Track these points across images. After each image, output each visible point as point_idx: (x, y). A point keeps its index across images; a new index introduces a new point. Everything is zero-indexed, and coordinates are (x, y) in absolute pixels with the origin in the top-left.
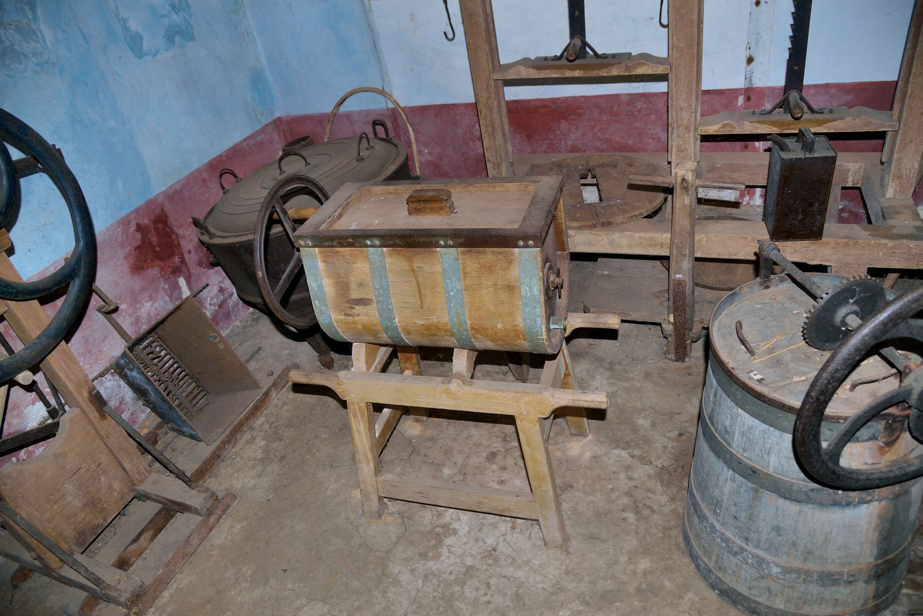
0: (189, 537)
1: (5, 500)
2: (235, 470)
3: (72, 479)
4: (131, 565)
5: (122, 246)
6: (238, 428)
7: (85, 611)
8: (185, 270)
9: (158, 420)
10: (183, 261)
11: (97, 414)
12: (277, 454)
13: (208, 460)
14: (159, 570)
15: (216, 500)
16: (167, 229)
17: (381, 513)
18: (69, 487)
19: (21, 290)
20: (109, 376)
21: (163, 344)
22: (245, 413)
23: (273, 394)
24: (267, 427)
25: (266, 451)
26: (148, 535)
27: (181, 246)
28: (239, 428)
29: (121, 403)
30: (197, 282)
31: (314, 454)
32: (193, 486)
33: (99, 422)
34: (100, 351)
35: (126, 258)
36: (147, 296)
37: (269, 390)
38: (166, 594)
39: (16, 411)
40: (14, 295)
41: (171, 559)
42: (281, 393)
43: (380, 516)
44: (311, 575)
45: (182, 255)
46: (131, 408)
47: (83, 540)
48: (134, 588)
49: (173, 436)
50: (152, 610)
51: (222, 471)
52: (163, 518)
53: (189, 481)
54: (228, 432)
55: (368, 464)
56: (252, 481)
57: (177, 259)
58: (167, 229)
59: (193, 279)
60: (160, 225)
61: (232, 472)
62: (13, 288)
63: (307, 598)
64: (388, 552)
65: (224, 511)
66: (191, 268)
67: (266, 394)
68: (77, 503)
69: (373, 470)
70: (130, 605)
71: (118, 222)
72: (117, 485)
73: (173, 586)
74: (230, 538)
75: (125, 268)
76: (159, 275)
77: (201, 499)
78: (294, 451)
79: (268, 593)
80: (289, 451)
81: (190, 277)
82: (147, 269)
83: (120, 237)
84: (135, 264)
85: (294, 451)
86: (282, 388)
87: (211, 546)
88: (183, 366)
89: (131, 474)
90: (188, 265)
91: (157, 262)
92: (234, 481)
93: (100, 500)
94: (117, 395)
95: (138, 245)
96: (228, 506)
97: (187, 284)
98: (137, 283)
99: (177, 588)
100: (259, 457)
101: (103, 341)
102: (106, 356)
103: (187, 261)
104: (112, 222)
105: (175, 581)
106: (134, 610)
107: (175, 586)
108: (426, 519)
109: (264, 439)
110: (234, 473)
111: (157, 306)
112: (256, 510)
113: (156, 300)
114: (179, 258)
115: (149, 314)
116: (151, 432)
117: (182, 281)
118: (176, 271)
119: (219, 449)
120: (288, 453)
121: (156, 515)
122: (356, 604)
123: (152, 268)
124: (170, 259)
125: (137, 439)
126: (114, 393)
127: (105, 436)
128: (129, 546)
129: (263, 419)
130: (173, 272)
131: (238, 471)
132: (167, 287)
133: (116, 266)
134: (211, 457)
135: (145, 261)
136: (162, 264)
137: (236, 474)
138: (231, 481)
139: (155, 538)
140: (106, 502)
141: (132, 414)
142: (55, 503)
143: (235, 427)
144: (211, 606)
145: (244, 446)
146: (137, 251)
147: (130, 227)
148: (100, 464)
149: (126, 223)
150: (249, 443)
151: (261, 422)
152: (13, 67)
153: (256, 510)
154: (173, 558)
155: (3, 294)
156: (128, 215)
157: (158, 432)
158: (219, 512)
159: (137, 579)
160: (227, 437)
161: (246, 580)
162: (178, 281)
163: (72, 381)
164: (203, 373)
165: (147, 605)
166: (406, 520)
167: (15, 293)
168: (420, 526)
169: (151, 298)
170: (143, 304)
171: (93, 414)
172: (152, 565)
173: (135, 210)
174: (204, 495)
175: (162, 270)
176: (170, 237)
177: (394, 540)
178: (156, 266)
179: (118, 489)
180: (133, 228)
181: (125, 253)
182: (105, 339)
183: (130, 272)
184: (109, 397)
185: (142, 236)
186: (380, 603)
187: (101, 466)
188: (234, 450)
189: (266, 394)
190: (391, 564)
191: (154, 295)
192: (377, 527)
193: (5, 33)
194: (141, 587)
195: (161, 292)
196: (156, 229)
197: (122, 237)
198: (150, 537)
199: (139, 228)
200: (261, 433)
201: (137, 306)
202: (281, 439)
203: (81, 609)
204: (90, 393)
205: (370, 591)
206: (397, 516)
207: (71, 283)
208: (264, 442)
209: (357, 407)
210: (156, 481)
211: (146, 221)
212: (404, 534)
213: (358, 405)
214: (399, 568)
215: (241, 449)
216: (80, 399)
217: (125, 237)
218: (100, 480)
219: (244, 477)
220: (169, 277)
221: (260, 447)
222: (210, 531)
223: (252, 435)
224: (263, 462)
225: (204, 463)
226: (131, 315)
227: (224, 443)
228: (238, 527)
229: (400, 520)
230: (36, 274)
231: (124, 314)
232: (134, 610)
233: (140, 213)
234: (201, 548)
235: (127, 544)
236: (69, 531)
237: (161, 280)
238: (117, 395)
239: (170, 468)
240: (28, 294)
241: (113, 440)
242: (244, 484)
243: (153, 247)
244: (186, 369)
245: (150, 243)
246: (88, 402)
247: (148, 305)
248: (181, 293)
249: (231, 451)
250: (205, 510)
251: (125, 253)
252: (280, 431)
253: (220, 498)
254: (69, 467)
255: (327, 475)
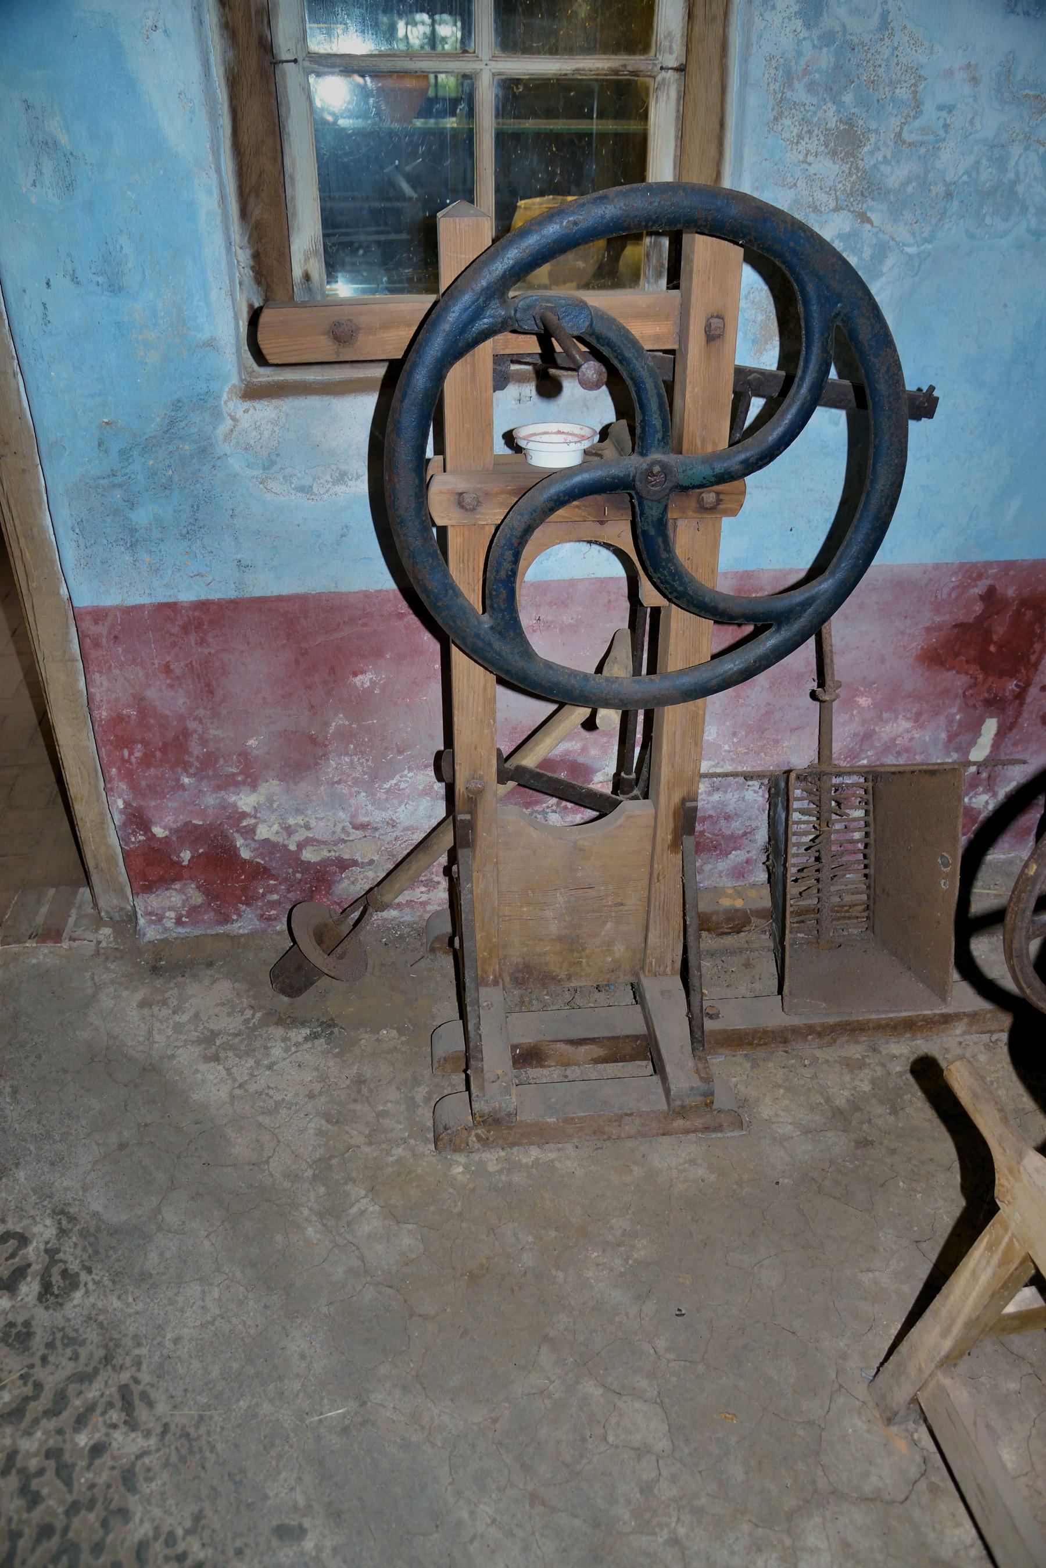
0: (626, 1114)
1: (474, 851)
2: (787, 1084)
3: (573, 892)
4: (542, 1066)
5: (937, 607)
6: (853, 1029)
7: (448, 1065)
8: (1010, 712)
9: (767, 903)
10: (1020, 696)
11: (670, 837)
12: (865, 1127)
13: (765, 1032)
14: (551, 1116)
15: (706, 1105)
16: (1037, 626)
17: (897, 1419)
18: (560, 899)
19: (691, 593)
20: (755, 784)
21: (871, 802)
22: (883, 1016)
23: (959, 1028)
24: (898, 1069)
25: (855, 1106)
26: (596, 1051)
27: (1037, 670)
28: (853, 1030)
29: (745, 834)
30: (1015, 744)
31: (915, 1190)
32: (698, 1053)
33: (663, 850)
34: (776, 742)
35: (928, 630)
36: (914, 710)
37: (957, 1016)
38: (535, 1152)
39: (605, 740)
40: (675, 594)
41: (578, 1118)
42: (975, 1037)
43: (889, 1421)
44: (701, 1368)
45: (1028, 684)
46: (754, 852)
47: (523, 978)
48: (500, 1108)
49: (766, 944)
50: (502, 1154)
51: (771, 1065)
52: (633, 1049)
53: (699, 1042)
54: (832, 1020)
55: (944, 1334)
56: (790, 1127)
57: (1012, 685)
58: (1037, 626)
59: (1015, 735)
60: (1030, 613)
61: (780, 1082)
62: (682, 583)
63: (659, 1393)
64: (836, 1494)
65: (707, 1129)
66: (1025, 715)
67: (946, 1019)
68: (554, 928)
69: (943, 1353)
70: (479, 1123)
71: (962, 565)
72: (619, 949)
73: (547, 1154)
74: (674, 1174)
75: (914, 645)
76: (960, 691)
77: (687, 1085)
78: (893, 1152)
79: (627, 1314)
80: (886, 1142)
81: (1011, 729)
82: (949, 670)
83: (946, 591)
84: (936, 649)
85: (893, 1152)
86: (982, 1033)
87: (644, 1156)
88: (873, 859)
89: (648, 952)
90: (1025, 707)
91: (974, 668)
92: (768, 1100)
93: (584, 949)
94: (750, 819)
95: (965, 621)
96: (719, 1128)
97: (996, 735)
98: (913, 679)
99: (552, 1161)
100: (837, 1102)
101: (792, 730)
102: (778, 754)
103: (1029, 700)
104: (951, 558)
105: (559, 1150)
106: (479, 1131)
107: (552, 1156)
108: (957, 1532)
109: (873, 1082)
110: (779, 1086)
111: (917, 736)
112: (746, 1177)
113: (922, 727)
114: (1017, 686)
115: (894, 740)
116: (744, 912)
117: (990, 727)
118: (994, 704)
119: (795, 1030)
120: (881, 1144)
121: (628, 1036)
122: (703, 1500)
123: (958, 672)
124: (1000, 677)
125: (688, 919)
126: (748, 814)
127: (655, 875)
128: (560, 1041)
129: (905, 1051)
130: (989, 703)
131: (788, 1090)
132: (958, 717)
133: (903, 633)
134: (773, 1032)
135: (956, 655)
136: (981, 677)
137: (782, 1091)
138: (764, 1095)
139: (602, 1063)
140: (588, 957)
141: (748, 862)
142: (529, 904)
143: (848, 1023)
144: (556, 1237)
145: (835, 1061)
146: (956, 631)
147: (976, 586)
148: (621, 904)
149: (975, 575)
150: (848, 1065)
151: (896, 1052)
152: (988, 221)
153: (746, 1177)
154: (582, 1120)
155: (662, 583)
156: (988, 564)
157: (753, 919)
158: (698, 1123)
159: (514, 1100)
160: (822, 1025)
161: (626, 1260)
162: (984, 721)
163: (673, 766)
164: (888, 894)
165: (500, 1142)
166: (922, 1485)
167: (679, 592)
168: (934, 1527)
169: (917, 717)
170: (897, 718)
171: (665, 834)
172: (553, 1100)
173: (1006, 562)
174: (696, 1082)
175: (974, 685)
176: (1031, 643)
177: (867, 1488)
178: (967, 673)
179: (617, 955)
180: (979, 589)
181: (933, 622)
182: (798, 728)
183: (917, 656)
184: (736, 814)
185: (984, 611)
186: (732, 1553)
187: (621, 908)
188: (818, 1053)
189: (946, 1019)
190: (818, 1519)
191: (924, 717)
192: (868, 1431)
193: (1020, 156)
194: (509, 1114)
195: (942, 720)
196: (1018, 615)
197: (949, 594)
198: (595, 1056)
199: (990, 596)
200: (878, 1068)
201: (885, 715)
202: (894, 1111)
203: (445, 1059)
204: (684, 801)
205: (743, 1514)
206: (918, 1459)
207: (773, 629)
208: (866, 1087)
209: (1006, 1239)
210: (669, 991)
211: (1011, 592)
212: (893, 1502)
213: (1011, 1240)
214: (823, 1545)
215: (827, 1062)
216: (663, 799)
217: (954, 595)
218: (604, 923)
219: (786, 1109)
220: (974, 706)
221: (855, 1088)
222: (664, 1135)
223: (864, 1057)
224: (834, 1116)
225: (755, 1031)
226: (864, 722)
227: (811, 1030)
228: (701, 1172)
229: (913, 1471)
230: (775, 570)
231: (855, 712)
232: (479, 1131)
233: (1012, 573)
234: (631, 1144)
235: (561, 1037)
236: (516, 955)
237: (958, 701)
238: (750, 819)
239: (692, 998)
240: (695, 606)
241: (662, 888)
242: (774, 1120)
243: (987, 639)
244: (872, 867)
245: (988, 632)
246: (671, 811)
247: (905, 725)
248: (973, 743)
249: (810, 1049)
250: (678, 1103)
251: (933, 622)
252: (907, 1097)
253: (714, 1106)
254: (580, 874)
255: (894, 1247)
